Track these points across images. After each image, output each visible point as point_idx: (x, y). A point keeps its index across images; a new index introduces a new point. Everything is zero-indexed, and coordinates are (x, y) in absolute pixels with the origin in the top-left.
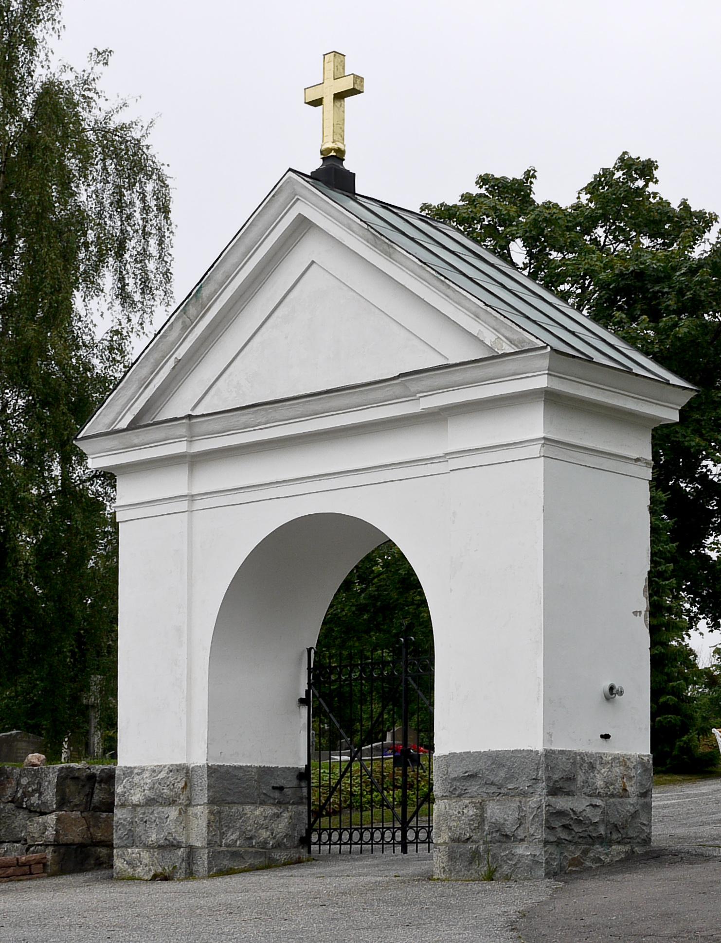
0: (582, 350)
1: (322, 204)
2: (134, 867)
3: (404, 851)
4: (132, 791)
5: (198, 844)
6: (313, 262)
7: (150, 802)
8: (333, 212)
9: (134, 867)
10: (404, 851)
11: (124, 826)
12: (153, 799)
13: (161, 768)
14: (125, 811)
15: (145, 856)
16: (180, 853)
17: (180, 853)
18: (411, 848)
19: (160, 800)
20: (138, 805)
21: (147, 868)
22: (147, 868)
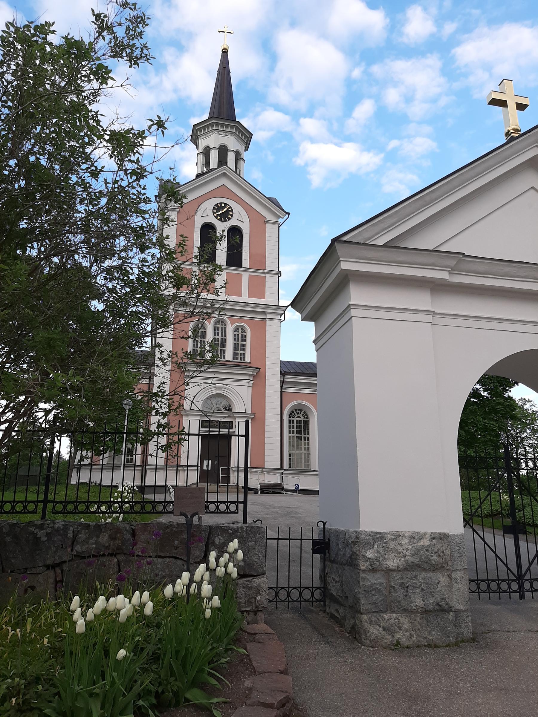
0: (519, 319)
1: (438, 193)
2: (392, 634)
3: (522, 597)
4: (386, 556)
5: (461, 607)
6: (289, 214)
7: (409, 567)
8: (427, 199)
9: (392, 634)
10: (522, 597)
11: (380, 591)
12: (417, 565)
13: (420, 536)
14: (377, 575)
15: (405, 621)
16: (451, 618)
17: (451, 618)
18: (528, 595)
19: (425, 566)
20: (394, 570)
21: (408, 634)
22: (408, 634)
